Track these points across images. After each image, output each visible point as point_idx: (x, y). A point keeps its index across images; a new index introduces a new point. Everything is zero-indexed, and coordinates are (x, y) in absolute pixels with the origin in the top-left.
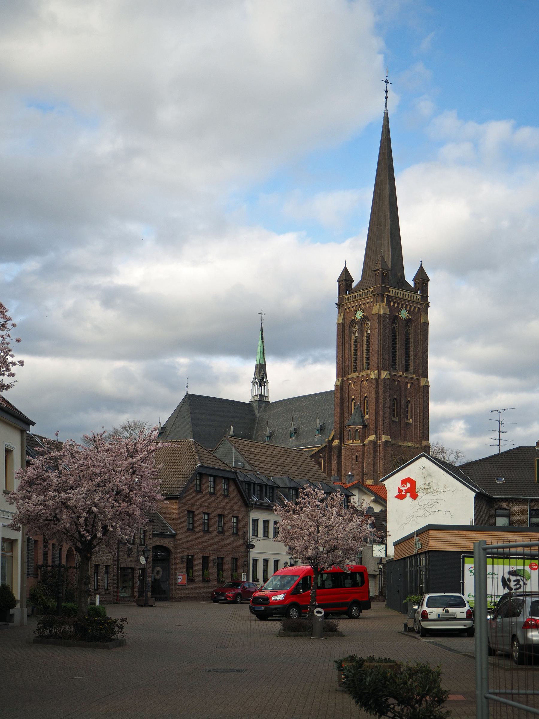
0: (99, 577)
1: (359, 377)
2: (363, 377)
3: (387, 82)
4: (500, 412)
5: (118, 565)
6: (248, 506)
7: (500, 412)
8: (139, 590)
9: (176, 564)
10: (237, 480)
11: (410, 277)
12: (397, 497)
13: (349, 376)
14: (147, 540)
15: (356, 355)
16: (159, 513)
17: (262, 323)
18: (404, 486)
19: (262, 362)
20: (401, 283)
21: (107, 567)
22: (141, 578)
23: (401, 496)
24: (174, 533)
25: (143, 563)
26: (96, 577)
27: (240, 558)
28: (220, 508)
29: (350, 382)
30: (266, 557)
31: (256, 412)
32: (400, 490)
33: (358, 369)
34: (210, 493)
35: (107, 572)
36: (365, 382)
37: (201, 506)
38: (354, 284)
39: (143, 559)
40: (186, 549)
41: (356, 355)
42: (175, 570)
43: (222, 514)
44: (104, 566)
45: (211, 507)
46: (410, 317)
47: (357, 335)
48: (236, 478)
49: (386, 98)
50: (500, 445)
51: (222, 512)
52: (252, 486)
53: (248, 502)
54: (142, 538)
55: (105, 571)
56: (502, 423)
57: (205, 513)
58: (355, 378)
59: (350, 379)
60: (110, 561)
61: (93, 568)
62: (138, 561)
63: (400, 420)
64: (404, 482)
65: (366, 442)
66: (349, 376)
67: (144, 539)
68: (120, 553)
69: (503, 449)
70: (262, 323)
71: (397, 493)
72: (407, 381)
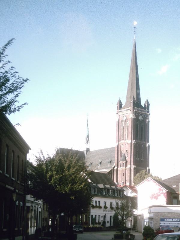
11: (143, 104)
15: (123, 134)
19: (88, 135)
20: (141, 107)
31: (85, 154)
33: (124, 139)
41: (123, 134)
52: (95, 189)
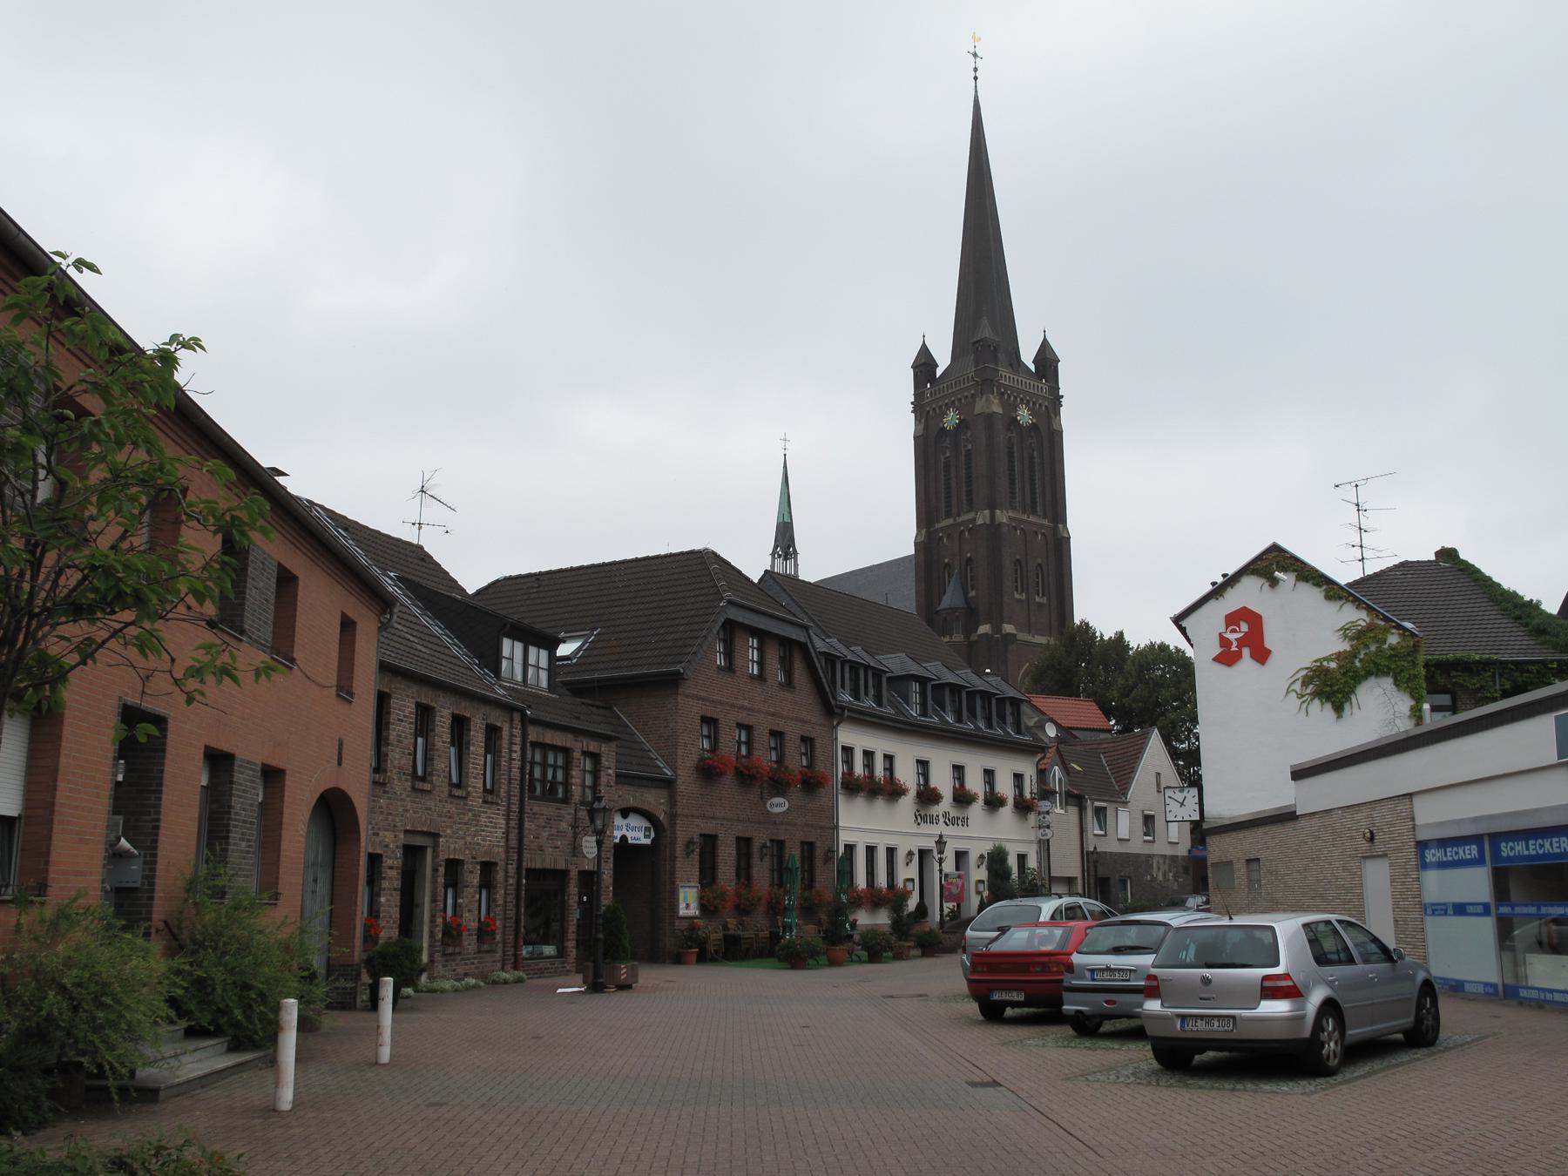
0: (460, 901)
1: (956, 525)
2: (962, 523)
3: (975, 55)
4: (1357, 486)
5: (520, 860)
6: (833, 713)
7: (1357, 486)
8: (578, 935)
9: (673, 858)
10: (810, 646)
11: (1028, 356)
12: (1218, 659)
13: (938, 526)
14: (603, 790)
16: (631, 723)
17: (785, 455)
18: (1233, 631)
21: (488, 868)
22: (585, 899)
23: (1227, 658)
24: (669, 774)
25: (590, 856)
26: (450, 901)
27: (818, 844)
28: (773, 715)
29: (940, 535)
30: (872, 840)
32: (1224, 642)
33: (954, 510)
34: (752, 677)
35: (487, 883)
36: (967, 533)
37: (733, 706)
38: (939, 372)
39: (588, 844)
40: (698, 817)
42: (673, 874)
43: (779, 730)
44: (477, 863)
45: (753, 711)
46: (1034, 421)
47: (948, 454)
48: (808, 642)
49: (976, 78)
50: (1363, 558)
51: (780, 725)
53: (833, 702)
54: (587, 783)
55: (481, 880)
56: (1364, 508)
57: (740, 726)
58: (948, 527)
59: (942, 529)
60: (496, 849)
61: (442, 870)
62: (576, 849)
63: (1028, 598)
64: (1232, 619)
65: (974, 638)
66: (938, 526)
67: (595, 787)
68: (527, 824)
69: (1372, 568)
70: (785, 455)
71: (1218, 651)
72: (1035, 529)
